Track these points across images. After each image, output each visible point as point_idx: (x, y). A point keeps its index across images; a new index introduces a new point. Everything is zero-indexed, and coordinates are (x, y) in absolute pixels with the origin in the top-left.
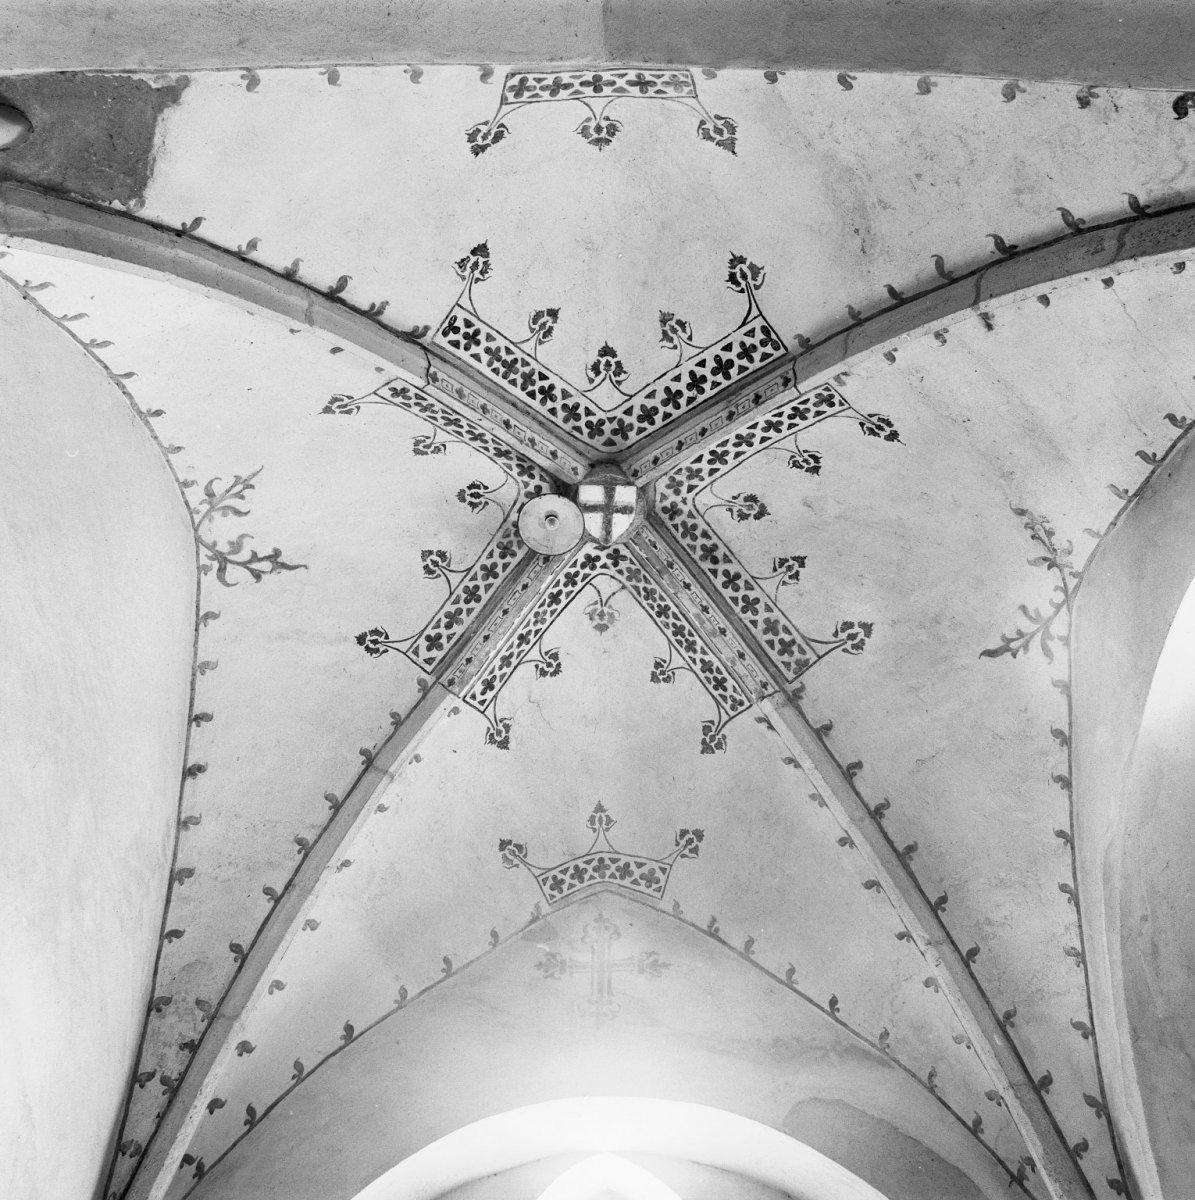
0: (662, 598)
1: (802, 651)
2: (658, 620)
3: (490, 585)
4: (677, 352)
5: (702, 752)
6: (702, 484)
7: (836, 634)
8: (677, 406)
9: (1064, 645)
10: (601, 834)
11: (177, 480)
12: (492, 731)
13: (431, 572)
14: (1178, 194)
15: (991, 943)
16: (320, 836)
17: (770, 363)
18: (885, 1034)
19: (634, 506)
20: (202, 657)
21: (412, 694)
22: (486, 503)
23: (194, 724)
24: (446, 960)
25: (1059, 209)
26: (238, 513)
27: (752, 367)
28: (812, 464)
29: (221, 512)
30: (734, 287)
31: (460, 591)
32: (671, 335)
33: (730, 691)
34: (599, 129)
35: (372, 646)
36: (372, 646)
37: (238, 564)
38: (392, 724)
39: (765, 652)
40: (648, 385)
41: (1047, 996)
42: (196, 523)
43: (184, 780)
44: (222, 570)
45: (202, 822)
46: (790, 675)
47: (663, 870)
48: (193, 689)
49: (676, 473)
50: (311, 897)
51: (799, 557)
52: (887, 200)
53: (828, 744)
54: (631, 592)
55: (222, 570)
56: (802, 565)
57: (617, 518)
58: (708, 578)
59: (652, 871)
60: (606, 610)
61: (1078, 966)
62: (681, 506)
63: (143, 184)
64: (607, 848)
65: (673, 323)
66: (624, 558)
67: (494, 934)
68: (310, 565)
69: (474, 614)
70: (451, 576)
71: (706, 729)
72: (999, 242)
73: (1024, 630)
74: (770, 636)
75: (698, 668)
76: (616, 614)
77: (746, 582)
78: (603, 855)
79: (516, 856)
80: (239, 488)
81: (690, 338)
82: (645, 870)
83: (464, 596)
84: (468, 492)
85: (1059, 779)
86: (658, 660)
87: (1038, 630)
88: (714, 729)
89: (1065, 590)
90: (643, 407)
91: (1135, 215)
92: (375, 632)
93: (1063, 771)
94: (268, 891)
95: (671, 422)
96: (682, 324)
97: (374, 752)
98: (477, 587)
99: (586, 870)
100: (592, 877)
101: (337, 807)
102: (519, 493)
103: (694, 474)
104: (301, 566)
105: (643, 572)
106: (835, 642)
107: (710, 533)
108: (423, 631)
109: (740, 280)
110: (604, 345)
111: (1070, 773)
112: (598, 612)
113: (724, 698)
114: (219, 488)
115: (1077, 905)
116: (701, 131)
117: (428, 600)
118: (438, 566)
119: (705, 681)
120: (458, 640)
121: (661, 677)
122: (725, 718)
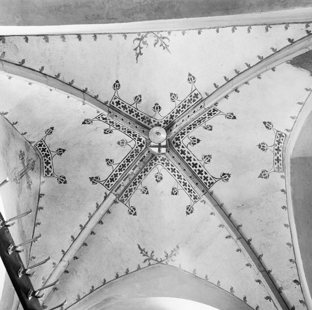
0: (132, 160)
1: (126, 200)
2: (125, 159)
3: (134, 116)
4: (202, 160)
5: (90, 178)
6: (164, 166)
7: (132, 207)
8: (187, 160)
9: (149, 265)
10: (56, 153)
11: (172, 31)
12: (89, 120)
13: (136, 98)
14: (275, 281)
15: (72, 276)
16: (61, 81)
17: (205, 185)
18: (34, 258)
19: (161, 153)
20: (113, 35)
21: (104, 100)
22: (155, 111)
23: (94, 35)
24: (17, 123)
25: (262, 254)
26: (155, 44)
27: (202, 180)
28: (174, 192)
29: (157, 39)
30: (222, 174)
31: (132, 108)
32: (206, 158)
33: (111, 183)
34: (263, 147)
35: (116, 85)
36: (116, 85)
37: (140, 44)
38: (95, 96)
39: (125, 191)
40: (191, 152)
41: (65, 296)
42: (155, 33)
43: (77, 34)
44: (138, 39)
45: (63, 42)
46: (120, 199)
47: (52, 175)
48: (104, 34)
49: (167, 160)
50: (46, 85)
51: (148, 192)
52: (253, 212)
53: (106, 214)
54: (131, 151)
55: (138, 39)
56: (147, 194)
57: (157, 149)
58: (140, 172)
59: (50, 171)
60: (125, 144)
61: (76, 300)
62: (157, 161)
63: (292, 64)
64: (53, 156)
65: (209, 158)
66: (141, 148)
67: (25, 133)
68: (137, 64)
69: (126, 113)
70: (135, 104)
71: (97, 178)
72: (250, 240)
73: (148, 254)
74: (128, 191)
75: (114, 173)
76: (123, 147)
77: (140, 181)
78: (50, 155)
79: (49, 132)
80: (164, 45)
81: (206, 163)
82: (50, 169)
83: (131, 109)
84: (158, 106)
85: (117, 275)
86: (113, 161)
87: (149, 257)
88: (98, 180)
89: (161, 261)
90: (185, 151)
91: (267, 272)
92: (119, 85)
93: (120, 275)
94: (43, 68)
95: (183, 159)
96: (209, 161)
97: (87, 92)
98: (133, 112)
99: (45, 152)
100: (43, 154)
101: (70, 84)
102: (159, 120)
103: (167, 164)
104: (137, 61)
105: (138, 154)
106: (130, 207)
107: (151, 169)
108: (121, 99)
109: (224, 176)
110: (200, 140)
111: (120, 277)
112: (124, 142)
113: (108, 182)
114: (165, 41)
115: (91, 293)
116: (264, 170)
117: (128, 98)
118: (137, 100)
119: (111, 175)
120: (119, 110)
121: (108, 162)
122: (103, 183)
